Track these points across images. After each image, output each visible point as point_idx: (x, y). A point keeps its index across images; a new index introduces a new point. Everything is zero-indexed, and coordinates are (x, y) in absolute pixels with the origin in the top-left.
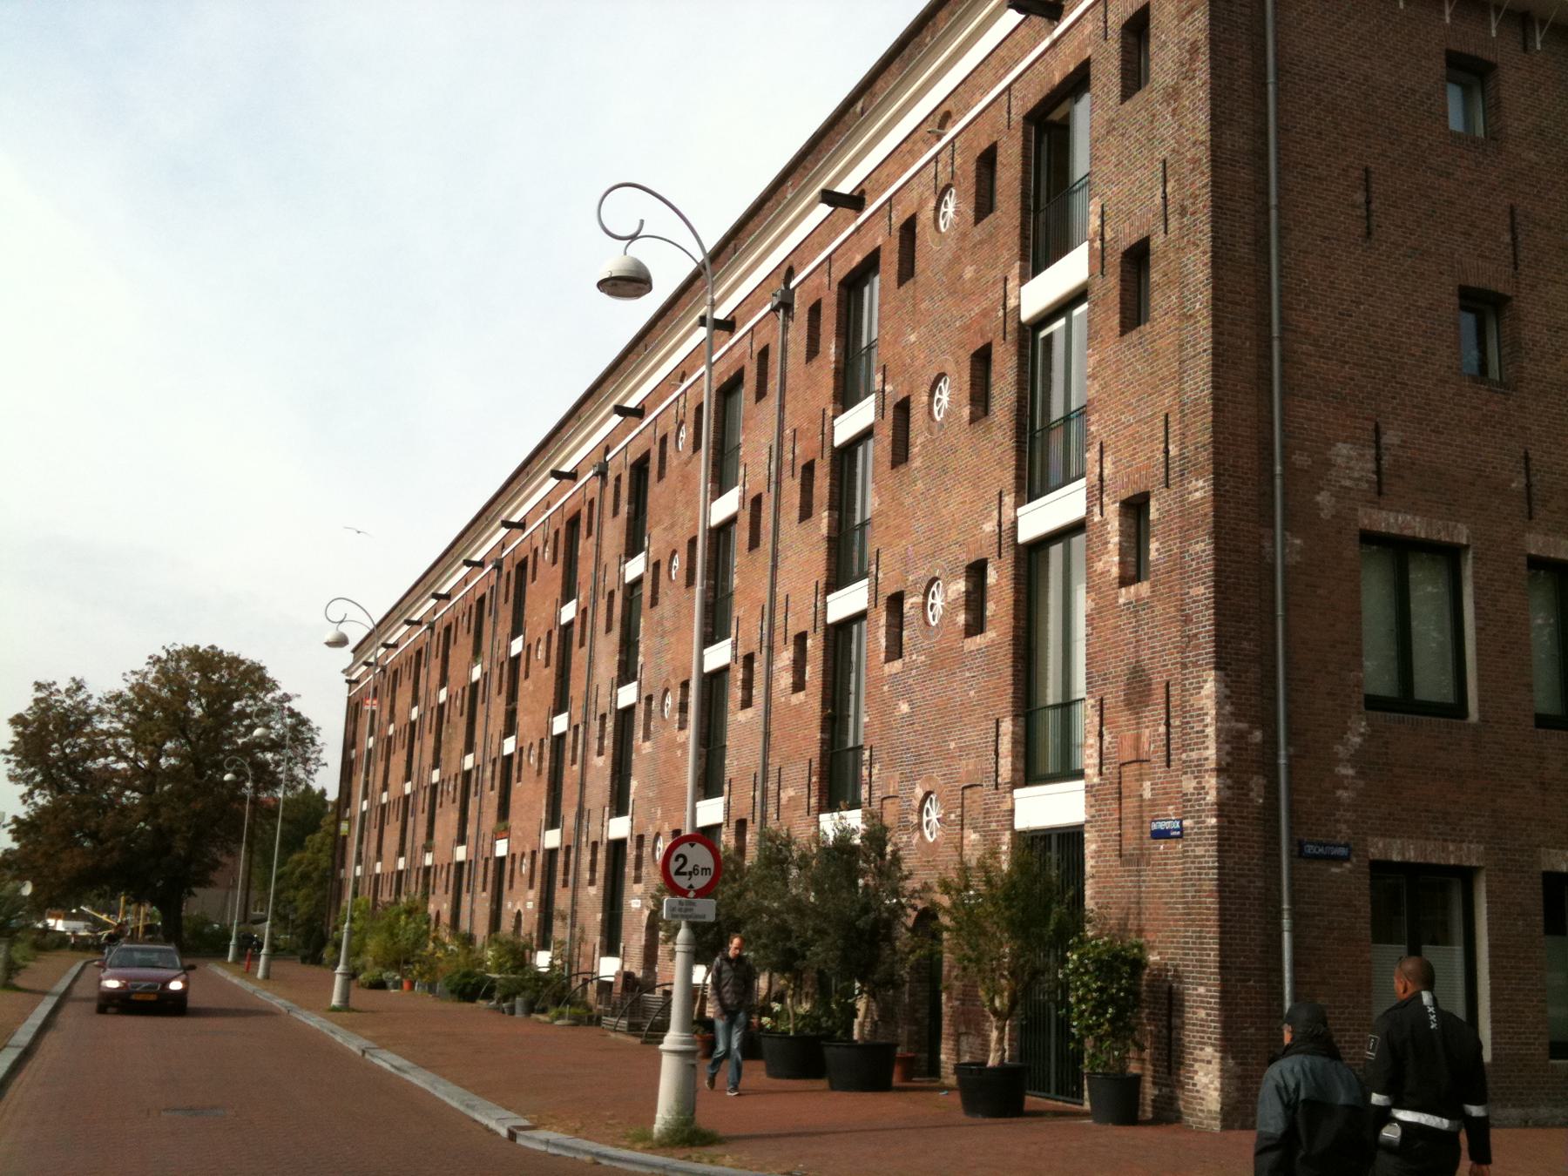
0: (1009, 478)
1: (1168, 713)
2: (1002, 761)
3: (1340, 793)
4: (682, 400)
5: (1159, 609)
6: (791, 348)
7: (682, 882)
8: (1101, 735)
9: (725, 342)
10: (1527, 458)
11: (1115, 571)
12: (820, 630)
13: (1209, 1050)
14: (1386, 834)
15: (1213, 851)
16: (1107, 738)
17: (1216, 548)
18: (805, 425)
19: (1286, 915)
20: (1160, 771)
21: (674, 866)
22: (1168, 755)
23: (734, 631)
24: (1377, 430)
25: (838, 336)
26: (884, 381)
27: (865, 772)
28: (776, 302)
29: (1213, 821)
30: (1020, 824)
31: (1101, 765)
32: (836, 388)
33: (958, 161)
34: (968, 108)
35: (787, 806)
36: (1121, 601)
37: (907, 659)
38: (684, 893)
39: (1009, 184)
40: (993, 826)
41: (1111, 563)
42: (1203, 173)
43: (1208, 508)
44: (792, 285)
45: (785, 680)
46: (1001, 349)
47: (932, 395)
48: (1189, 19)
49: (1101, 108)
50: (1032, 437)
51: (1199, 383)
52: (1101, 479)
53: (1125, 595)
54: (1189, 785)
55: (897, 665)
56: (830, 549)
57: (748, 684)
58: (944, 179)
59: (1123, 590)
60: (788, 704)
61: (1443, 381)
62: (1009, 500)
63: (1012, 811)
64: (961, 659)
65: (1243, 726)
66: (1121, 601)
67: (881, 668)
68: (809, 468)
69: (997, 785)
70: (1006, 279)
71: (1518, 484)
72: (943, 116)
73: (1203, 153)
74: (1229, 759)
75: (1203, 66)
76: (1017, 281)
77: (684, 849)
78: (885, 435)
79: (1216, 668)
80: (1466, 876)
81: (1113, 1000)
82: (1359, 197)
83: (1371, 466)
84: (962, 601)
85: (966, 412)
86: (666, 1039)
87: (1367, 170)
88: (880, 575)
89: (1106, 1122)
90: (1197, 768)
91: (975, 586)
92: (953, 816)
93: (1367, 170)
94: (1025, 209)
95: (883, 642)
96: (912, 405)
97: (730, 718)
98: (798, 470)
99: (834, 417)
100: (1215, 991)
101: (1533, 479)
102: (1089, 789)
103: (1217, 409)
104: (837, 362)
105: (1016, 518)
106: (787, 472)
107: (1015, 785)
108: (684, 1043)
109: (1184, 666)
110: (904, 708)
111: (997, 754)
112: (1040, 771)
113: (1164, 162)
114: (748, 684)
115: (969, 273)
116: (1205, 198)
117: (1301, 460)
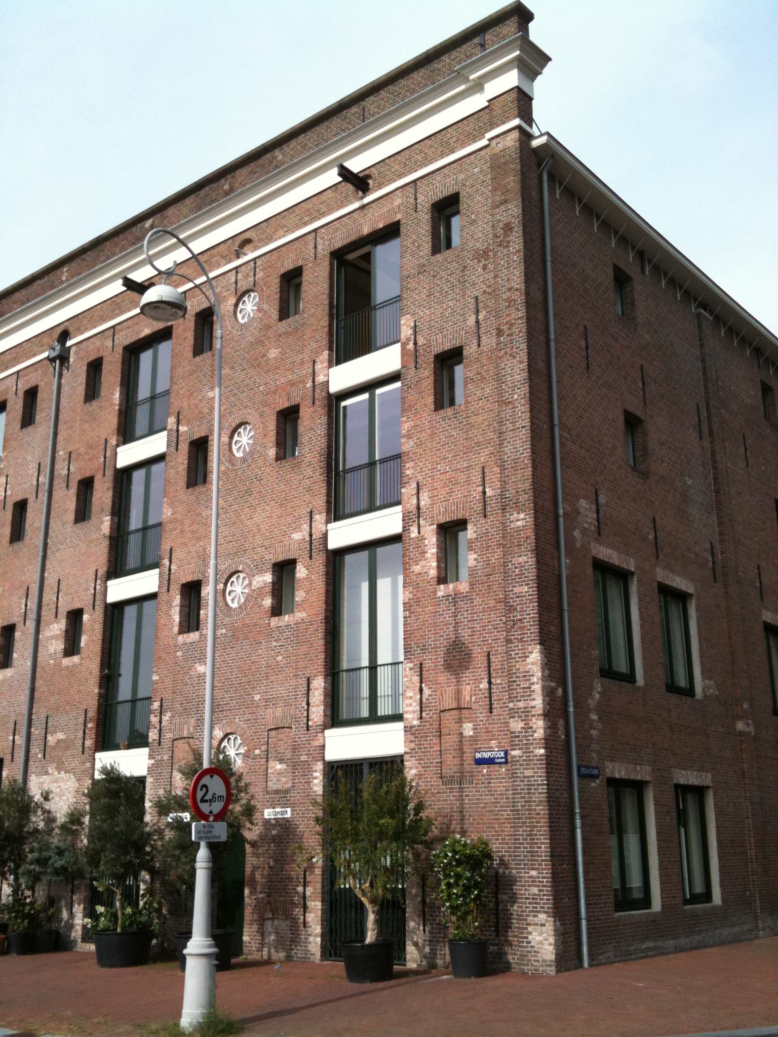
0: (320, 501)
1: (489, 674)
2: (312, 709)
5: (477, 600)
6: (65, 389)
7: (205, 808)
8: (421, 690)
11: (433, 573)
13: (542, 917)
15: (542, 772)
16: (427, 692)
19: (578, 817)
20: (482, 715)
21: (200, 794)
25: (122, 385)
26: (178, 423)
27: (154, 719)
28: (54, 354)
29: (542, 751)
31: (421, 711)
32: (119, 424)
33: (260, 275)
34: (270, 239)
35: (54, 748)
36: (440, 594)
38: (205, 817)
39: (316, 297)
41: (430, 565)
43: (530, 533)
44: (69, 344)
47: (231, 437)
48: (503, 208)
49: (412, 255)
51: (519, 446)
52: (418, 508)
54: (517, 725)
56: (111, 545)
58: (243, 285)
59: (442, 587)
60: (58, 665)
61: (620, 467)
62: (320, 518)
63: (324, 746)
64: (269, 634)
66: (440, 594)
67: (175, 638)
68: (86, 485)
69: (308, 727)
70: (314, 362)
72: (243, 242)
73: (519, 298)
75: (516, 241)
76: (326, 364)
77: (206, 780)
78: (181, 461)
79: (541, 644)
81: (476, 885)
82: (583, 344)
83: (595, 516)
84: (269, 589)
85: (272, 452)
86: (189, 944)
87: (585, 327)
88: (173, 567)
89: (469, 977)
90: (526, 714)
91: (278, 579)
92: (257, 752)
93: (585, 327)
94: (331, 315)
95: (177, 618)
99: (117, 446)
100: (547, 873)
101: (658, 534)
102: (407, 730)
103: (534, 467)
104: (120, 405)
105: (327, 531)
106: (59, 484)
107: (325, 727)
108: (210, 946)
109: (508, 641)
111: (308, 704)
112: (344, 715)
113: (477, 298)
115: (273, 353)
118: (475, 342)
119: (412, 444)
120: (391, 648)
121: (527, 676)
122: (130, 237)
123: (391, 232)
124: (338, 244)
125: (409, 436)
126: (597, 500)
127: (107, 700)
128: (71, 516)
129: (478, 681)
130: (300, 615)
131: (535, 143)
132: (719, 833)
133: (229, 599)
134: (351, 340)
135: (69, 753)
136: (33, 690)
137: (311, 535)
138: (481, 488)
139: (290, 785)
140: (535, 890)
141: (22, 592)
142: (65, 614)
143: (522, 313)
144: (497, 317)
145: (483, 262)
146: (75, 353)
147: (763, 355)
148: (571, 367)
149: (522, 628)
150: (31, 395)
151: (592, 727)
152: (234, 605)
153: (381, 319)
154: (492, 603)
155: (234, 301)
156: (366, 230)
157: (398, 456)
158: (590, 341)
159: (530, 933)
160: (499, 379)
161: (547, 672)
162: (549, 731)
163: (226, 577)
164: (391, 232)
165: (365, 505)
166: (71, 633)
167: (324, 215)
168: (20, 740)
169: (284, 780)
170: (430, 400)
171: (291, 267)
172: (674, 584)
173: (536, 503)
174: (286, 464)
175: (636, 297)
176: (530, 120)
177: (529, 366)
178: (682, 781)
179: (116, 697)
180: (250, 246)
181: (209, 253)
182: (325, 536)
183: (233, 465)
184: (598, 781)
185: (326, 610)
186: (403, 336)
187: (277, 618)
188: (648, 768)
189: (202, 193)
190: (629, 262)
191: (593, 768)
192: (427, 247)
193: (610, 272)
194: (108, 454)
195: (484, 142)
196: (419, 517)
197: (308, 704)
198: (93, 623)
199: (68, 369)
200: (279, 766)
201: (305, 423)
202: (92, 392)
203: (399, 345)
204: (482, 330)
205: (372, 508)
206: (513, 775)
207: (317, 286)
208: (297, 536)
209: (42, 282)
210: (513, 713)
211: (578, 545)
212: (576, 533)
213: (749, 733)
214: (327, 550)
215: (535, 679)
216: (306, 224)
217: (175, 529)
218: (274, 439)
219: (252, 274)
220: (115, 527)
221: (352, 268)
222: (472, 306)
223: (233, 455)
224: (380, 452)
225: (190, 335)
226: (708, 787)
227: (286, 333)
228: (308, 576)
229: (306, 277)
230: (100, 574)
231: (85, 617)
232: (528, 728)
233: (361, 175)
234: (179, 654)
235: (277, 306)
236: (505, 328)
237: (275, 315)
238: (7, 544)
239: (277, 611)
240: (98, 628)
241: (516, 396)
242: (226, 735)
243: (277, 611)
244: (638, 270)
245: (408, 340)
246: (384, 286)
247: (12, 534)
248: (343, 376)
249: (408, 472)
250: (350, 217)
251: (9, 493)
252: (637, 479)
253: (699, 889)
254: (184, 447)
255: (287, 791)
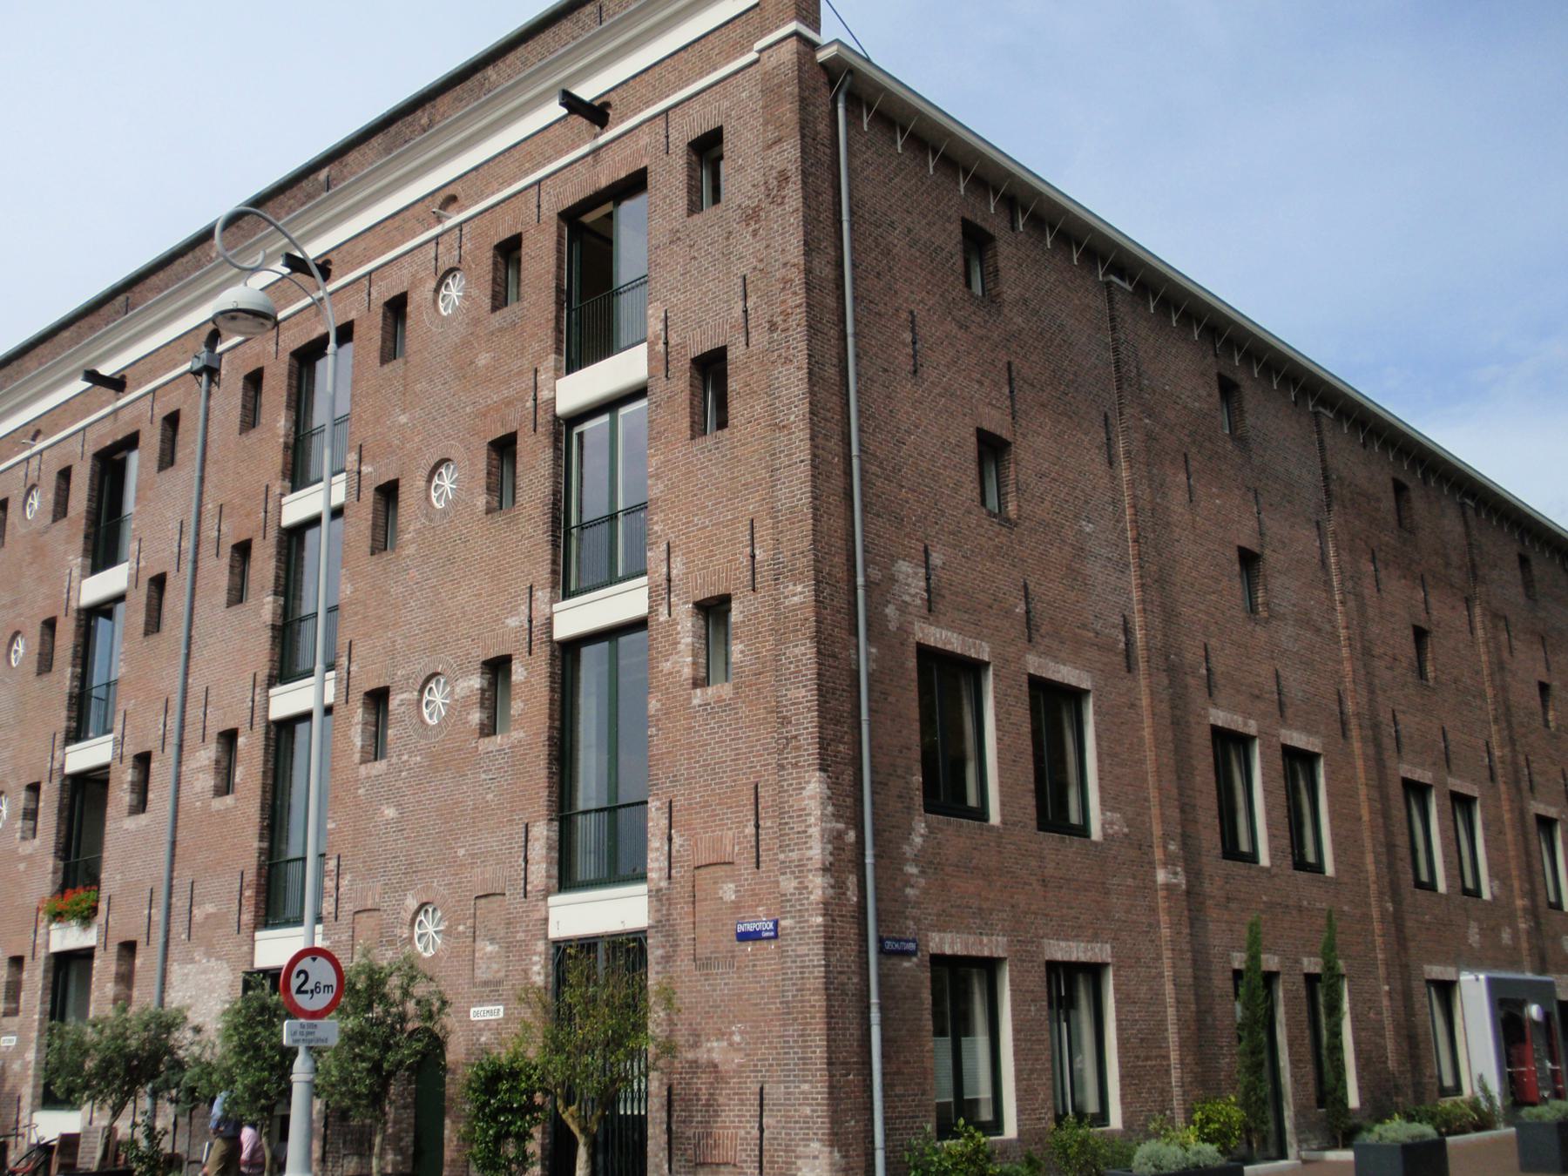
0: (543, 572)
2: (531, 868)
3: (909, 891)
4: (35, 463)
5: (744, 710)
6: (215, 415)
8: (670, 839)
9: (108, 403)
10: (1026, 587)
11: (687, 672)
12: (260, 729)
14: (942, 929)
15: (819, 949)
16: (677, 840)
17: (819, 652)
18: (237, 501)
22: (758, 856)
23: (118, 726)
24: (926, 551)
25: (288, 407)
28: (198, 365)
29: (820, 920)
30: (555, 933)
31: (670, 868)
33: (467, 246)
35: (202, 925)
36: (696, 702)
37: (394, 760)
40: (520, 936)
42: (795, 293)
44: (219, 349)
45: (200, 779)
46: (531, 441)
47: (430, 480)
48: (776, 149)
50: (568, 533)
51: (795, 489)
53: (698, 696)
54: (788, 884)
55: (380, 766)
56: (274, 638)
57: (141, 789)
58: (446, 262)
59: (698, 691)
62: (542, 595)
63: (546, 920)
65: (841, 826)
66: (696, 702)
68: (243, 550)
71: (1020, 609)
72: (448, 199)
73: (798, 279)
74: (831, 859)
75: (793, 195)
76: (551, 374)
80: (990, 966)
82: (908, 337)
83: (923, 584)
84: (476, 698)
85: (481, 501)
90: (800, 868)
91: (490, 684)
92: (461, 928)
93: (911, 313)
94: (559, 303)
95: (358, 742)
96: (401, 490)
97: (110, 826)
98: (226, 551)
99: (282, 495)
100: (822, 1088)
104: (287, 436)
105: (552, 614)
106: (207, 550)
109: (782, 767)
110: (390, 812)
111: (526, 861)
112: (579, 877)
114: (141, 789)
115: (483, 359)
116: (798, 318)
117: (876, 574)
118: (743, 339)
119: (661, 487)
120: (565, 780)
121: (802, 814)
122: (300, 195)
123: (635, 184)
124: (569, 202)
125: (657, 476)
126: (927, 562)
127: (270, 857)
128: (223, 597)
129: (741, 824)
130: (517, 735)
131: (822, 56)
132: (1120, 1029)
133: (426, 712)
134: (588, 337)
135: (220, 932)
136: (174, 844)
137: (530, 621)
138: (748, 550)
139: (502, 974)
140: (808, 1110)
141: (161, 704)
142: (215, 736)
143: (800, 299)
144: (770, 304)
145: (753, 226)
146: (231, 362)
147: (1220, 336)
148: (885, 370)
149: (797, 748)
150: (172, 421)
151: (907, 884)
152: (433, 722)
153: (626, 306)
154: (762, 713)
155: (433, 284)
156: (604, 182)
157: (643, 506)
158: (922, 331)
159: (799, 1169)
160: (771, 391)
161: (830, 808)
162: (830, 892)
163: (421, 681)
164: (635, 184)
165: (606, 578)
166: (224, 764)
167: (549, 160)
168: (158, 915)
169: (495, 966)
170: (686, 423)
171: (507, 235)
172: (1057, 677)
173: (817, 571)
174: (499, 518)
175: (1001, 265)
176: (815, 25)
177: (810, 373)
178: (1059, 957)
179: (287, 853)
180: (454, 206)
181: (401, 216)
182: (549, 623)
183: (431, 520)
184: (915, 959)
185: (550, 727)
186: (650, 331)
187: (487, 740)
188: (1003, 940)
189: (393, 129)
190: (990, 214)
191: (907, 941)
192: (682, 204)
193: (956, 229)
194: (270, 507)
195: (753, 56)
196: (669, 592)
197: (526, 861)
198: (251, 747)
199: (218, 385)
200: (489, 948)
201: (525, 459)
202: (250, 418)
203: (645, 345)
204: (752, 323)
205: (613, 580)
206: (782, 952)
207: (542, 259)
208: (513, 622)
209: (184, 260)
210: (784, 868)
211: (892, 626)
212: (890, 611)
213: (1176, 885)
214: (551, 641)
215: (812, 820)
216: (526, 174)
217: (356, 614)
218: (483, 482)
219: (456, 245)
220: (279, 611)
221: (588, 233)
222: (739, 290)
223: (432, 506)
224: (625, 501)
225: (377, 336)
226: (1105, 965)
227: (500, 330)
228: (530, 677)
229: (527, 250)
230: (259, 678)
231: (241, 741)
232: (802, 888)
233: (596, 103)
234: (361, 791)
235: (489, 292)
236: (779, 320)
237: (487, 302)
238: (141, 638)
239: (489, 728)
240: (258, 755)
241: (792, 418)
242: (422, 905)
243: (489, 728)
244: (1005, 223)
245: (657, 337)
246: (630, 258)
247: (147, 624)
248: (576, 390)
249: (656, 528)
250: (578, 165)
251: (142, 564)
252: (997, 528)
253: (1092, 1107)
254: (368, 495)
255: (499, 983)
